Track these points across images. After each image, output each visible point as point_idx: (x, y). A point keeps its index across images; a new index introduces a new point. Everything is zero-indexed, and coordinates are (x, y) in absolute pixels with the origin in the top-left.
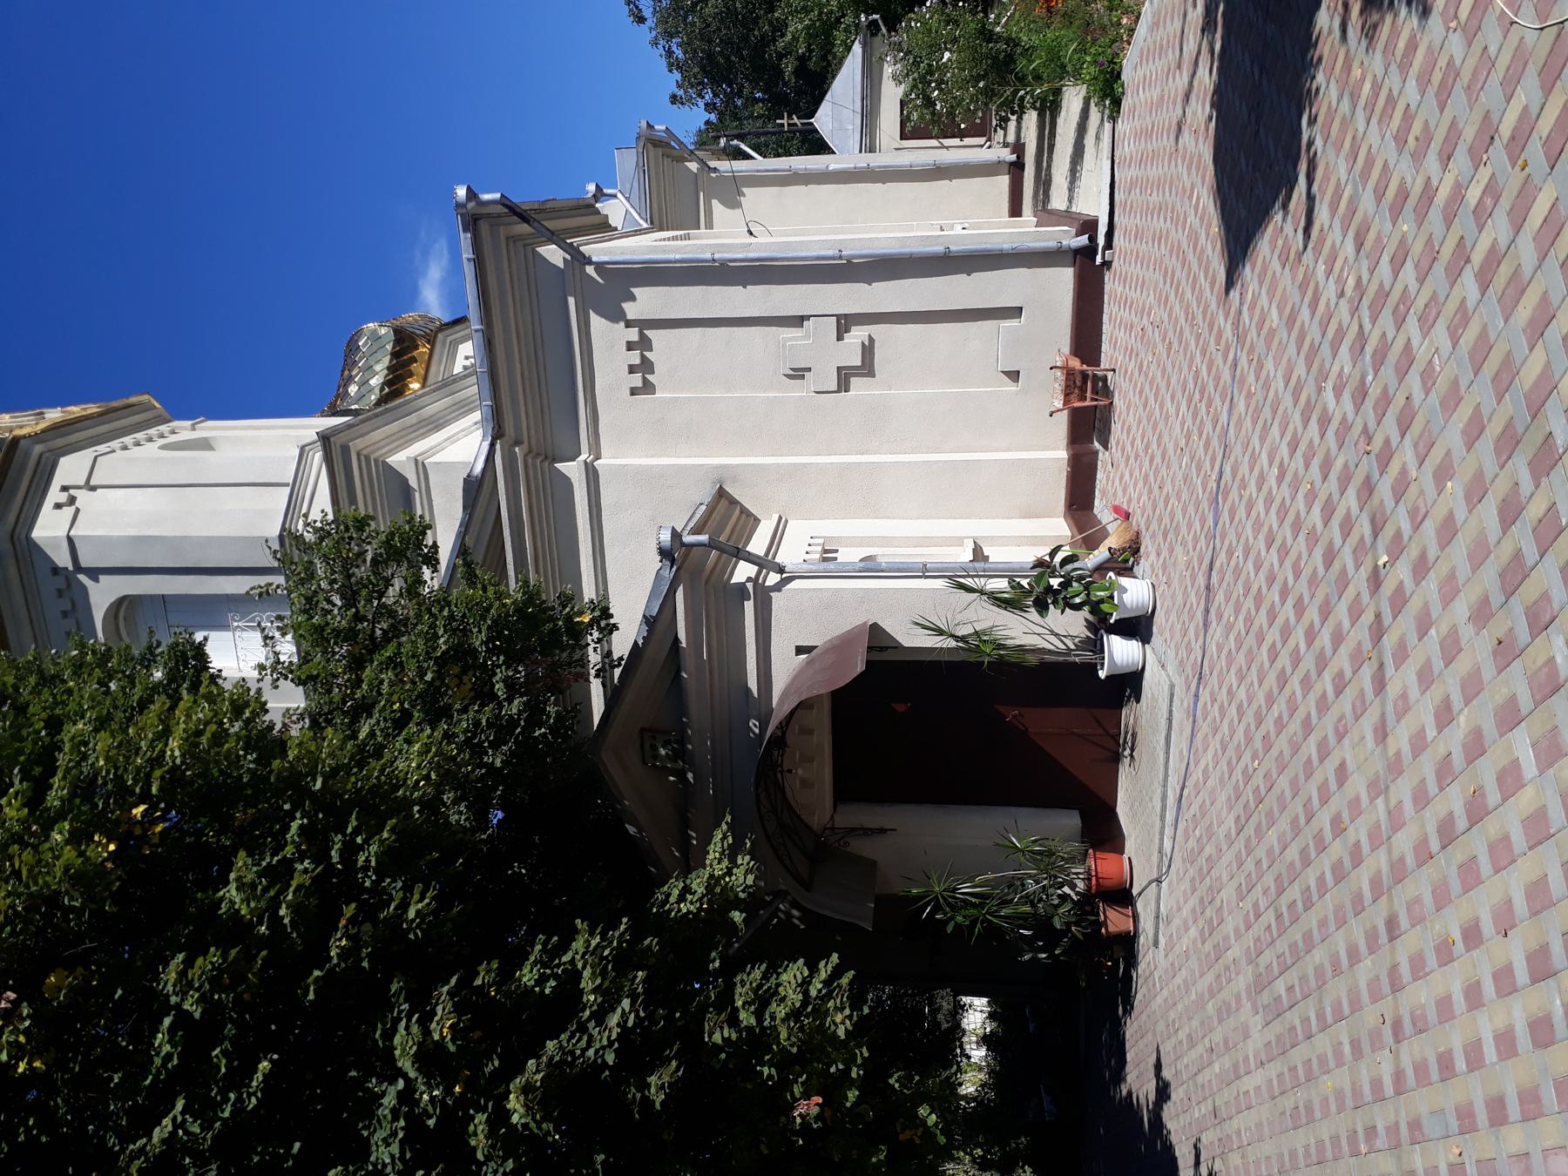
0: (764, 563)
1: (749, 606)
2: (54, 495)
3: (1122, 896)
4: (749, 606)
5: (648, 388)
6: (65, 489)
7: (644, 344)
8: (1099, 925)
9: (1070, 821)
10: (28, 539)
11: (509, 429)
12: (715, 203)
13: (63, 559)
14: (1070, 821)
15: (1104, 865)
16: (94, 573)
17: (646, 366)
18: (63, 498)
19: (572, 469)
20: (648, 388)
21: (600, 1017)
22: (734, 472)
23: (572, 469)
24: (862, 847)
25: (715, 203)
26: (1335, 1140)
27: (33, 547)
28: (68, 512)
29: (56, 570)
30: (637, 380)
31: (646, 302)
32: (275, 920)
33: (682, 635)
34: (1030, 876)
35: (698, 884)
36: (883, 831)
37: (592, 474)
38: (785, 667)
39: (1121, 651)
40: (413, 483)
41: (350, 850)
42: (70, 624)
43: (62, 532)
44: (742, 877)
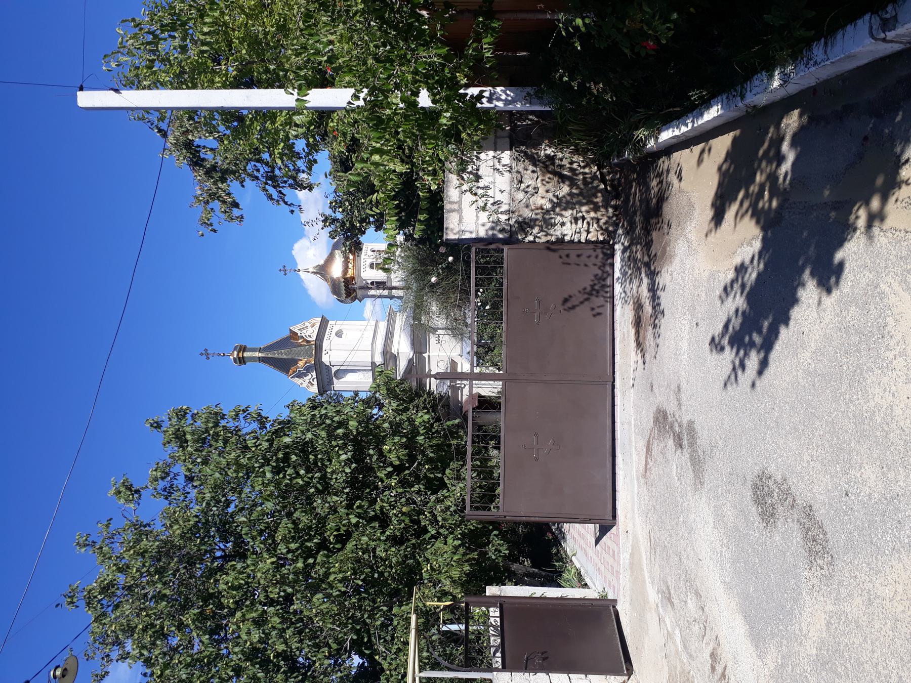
2: (324, 352)
13: (328, 364)
19: (426, 355)
23: (426, 355)
28: (327, 355)
37: (429, 356)
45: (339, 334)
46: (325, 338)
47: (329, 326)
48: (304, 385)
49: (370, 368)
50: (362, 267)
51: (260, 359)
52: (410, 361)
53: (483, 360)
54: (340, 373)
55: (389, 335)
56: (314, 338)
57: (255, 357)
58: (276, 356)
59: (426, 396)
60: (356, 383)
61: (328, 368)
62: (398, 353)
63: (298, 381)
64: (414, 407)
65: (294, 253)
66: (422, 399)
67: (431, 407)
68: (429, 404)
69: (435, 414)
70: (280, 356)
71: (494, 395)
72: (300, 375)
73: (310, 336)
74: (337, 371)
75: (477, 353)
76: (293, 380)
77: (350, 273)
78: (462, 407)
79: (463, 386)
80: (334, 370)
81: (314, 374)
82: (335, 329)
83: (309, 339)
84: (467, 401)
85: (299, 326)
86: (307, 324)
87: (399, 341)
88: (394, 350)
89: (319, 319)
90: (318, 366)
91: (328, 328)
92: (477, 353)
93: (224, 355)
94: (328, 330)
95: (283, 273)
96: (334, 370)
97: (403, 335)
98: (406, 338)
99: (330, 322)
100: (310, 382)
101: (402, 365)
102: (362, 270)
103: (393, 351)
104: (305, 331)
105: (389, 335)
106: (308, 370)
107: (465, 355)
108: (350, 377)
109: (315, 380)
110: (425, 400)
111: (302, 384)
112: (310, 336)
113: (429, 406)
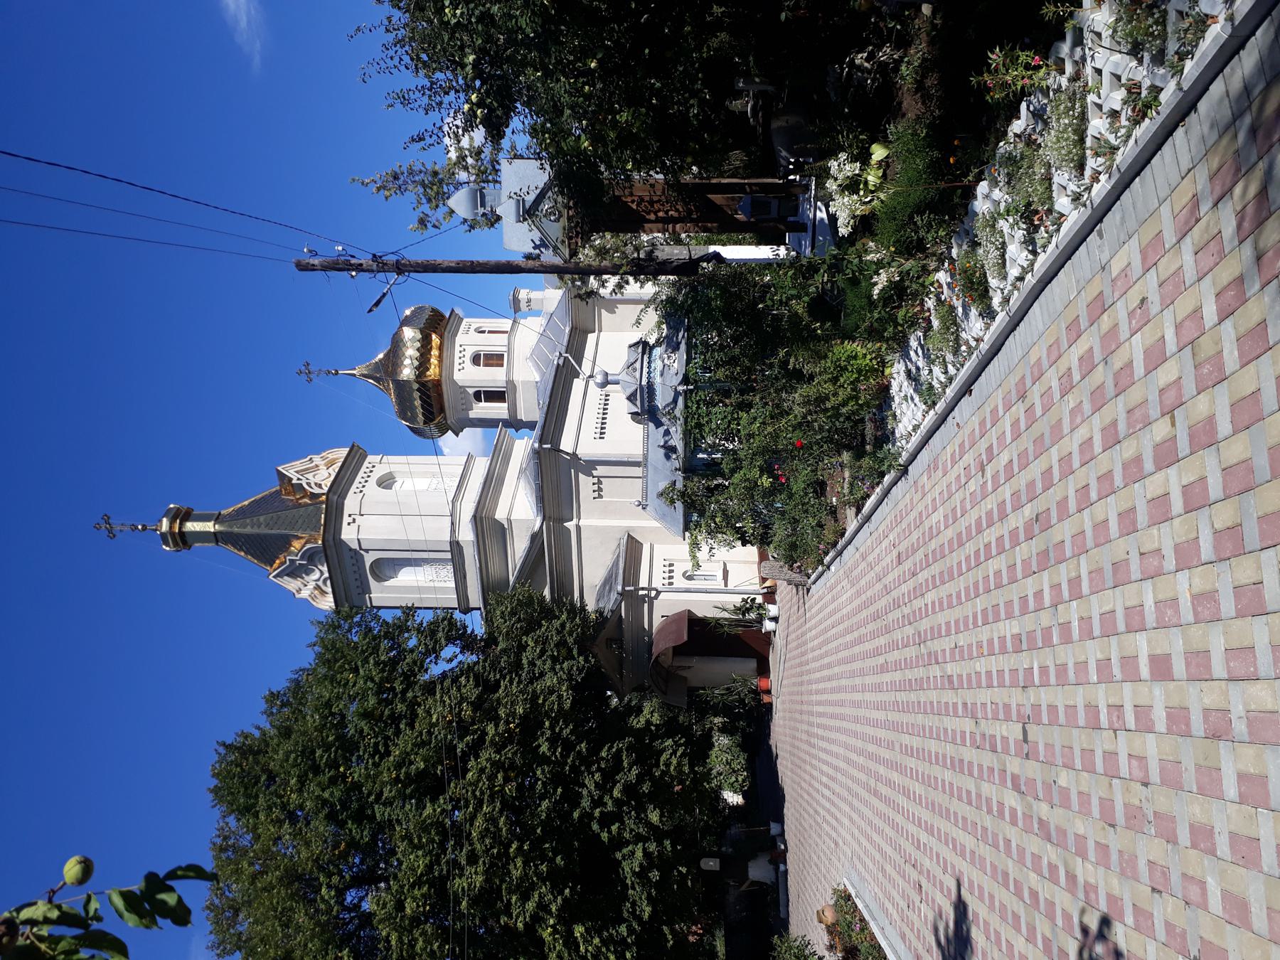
0: (650, 589)
1: (646, 605)
2: (346, 519)
3: (769, 692)
4: (646, 605)
5: (600, 496)
6: (350, 516)
7: (600, 482)
8: (761, 700)
9: (752, 664)
10: (340, 539)
11: (547, 515)
12: (603, 311)
13: (355, 546)
14: (752, 664)
15: (763, 684)
16: (367, 551)
17: (600, 489)
18: (350, 520)
19: (570, 525)
20: (600, 496)
21: (629, 771)
22: (633, 528)
23: (570, 525)
24: (684, 673)
25: (603, 311)
26: (948, 624)
27: (342, 542)
28: (354, 526)
29: (351, 549)
30: (596, 494)
31: (601, 470)
32: (556, 757)
33: (623, 615)
34: (793, 297)
35: (642, 720)
36: (689, 667)
37: (578, 528)
38: (657, 621)
39: (768, 626)
40: (506, 526)
41: (561, 729)
42: (355, 568)
43: (354, 536)
44: (656, 719)
45: (386, 482)
46: (353, 489)
47: (366, 464)
48: (305, 594)
49: (449, 556)
50: (457, 361)
51: (216, 537)
52: (535, 538)
53: (702, 514)
54: (386, 568)
55: (492, 484)
56: (326, 489)
57: (208, 533)
58: (248, 530)
59: (564, 617)
60: (419, 589)
61: (356, 556)
62: (509, 521)
63: (291, 584)
64: (536, 642)
65: (772, 742)
66: (556, 623)
67: (575, 642)
68: (570, 634)
69: (586, 660)
70: (256, 531)
71: (726, 615)
72: (294, 572)
73: (320, 486)
74: (377, 564)
75: (683, 495)
76: (278, 581)
77: (433, 372)
78: (651, 644)
79: (653, 593)
80: (369, 559)
81: (325, 569)
82: (380, 471)
83: (317, 490)
84: (661, 630)
85: (299, 465)
86: (317, 459)
87: (514, 497)
88: (500, 515)
89: (344, 452)
90: (330, 552)
91: (363, 469)
92: (683, 495)
93: (144, 528)
94: (361, 474)
95: (304, 377)
96: (369, 559)
97: (522, 483)
98: (529, 492)
99: (370, 458)
100: (318, 587)
101: (519, 547)
102: (457, 367)
103: (497, 517)
104: (310, 476)
105: (492, 484)
106: (311, 557)
107: (653, 501)
108: (406, 577)
109: (328, 582)
110: (563, 625)
111: (299, 591)
112: (320, 486)
113: (570, 640)
